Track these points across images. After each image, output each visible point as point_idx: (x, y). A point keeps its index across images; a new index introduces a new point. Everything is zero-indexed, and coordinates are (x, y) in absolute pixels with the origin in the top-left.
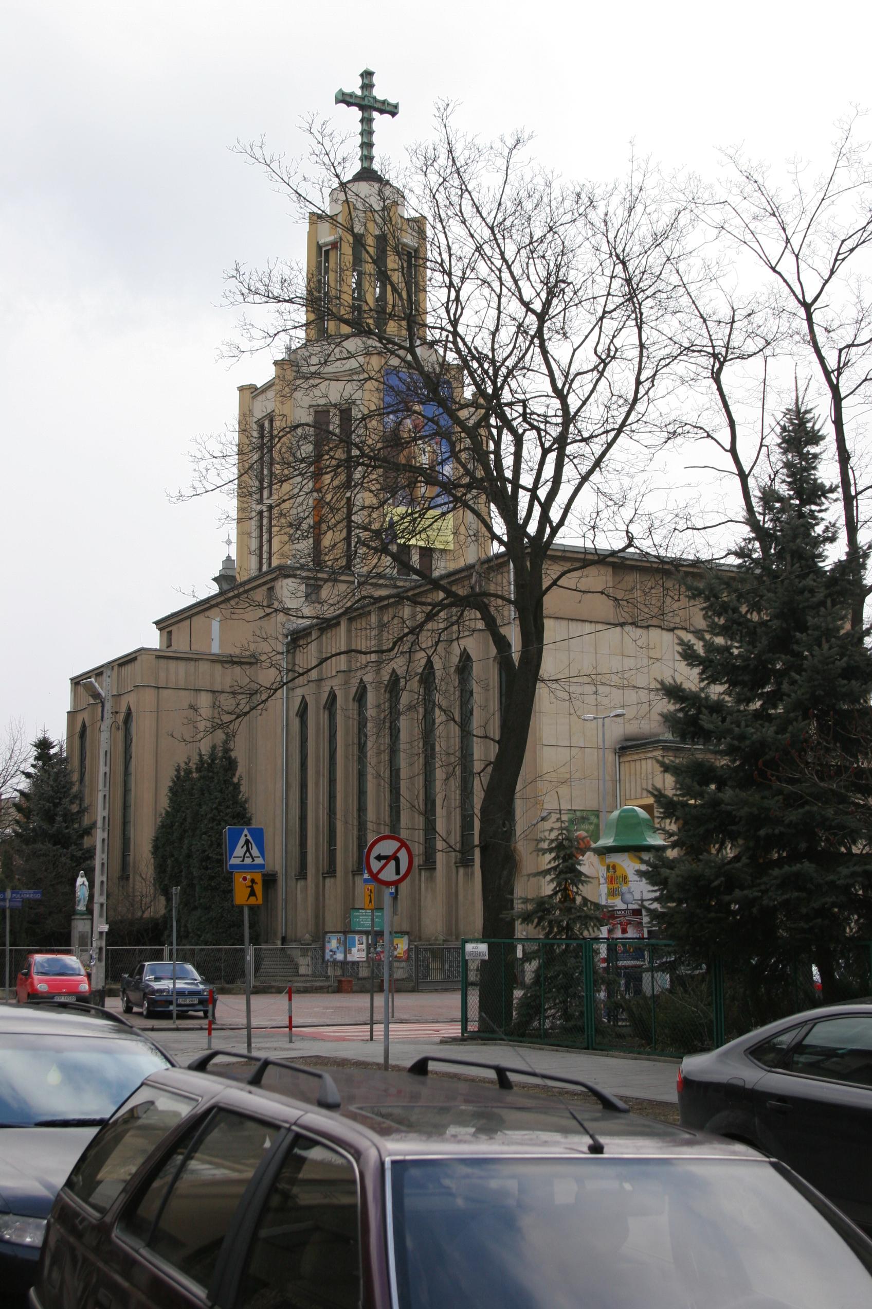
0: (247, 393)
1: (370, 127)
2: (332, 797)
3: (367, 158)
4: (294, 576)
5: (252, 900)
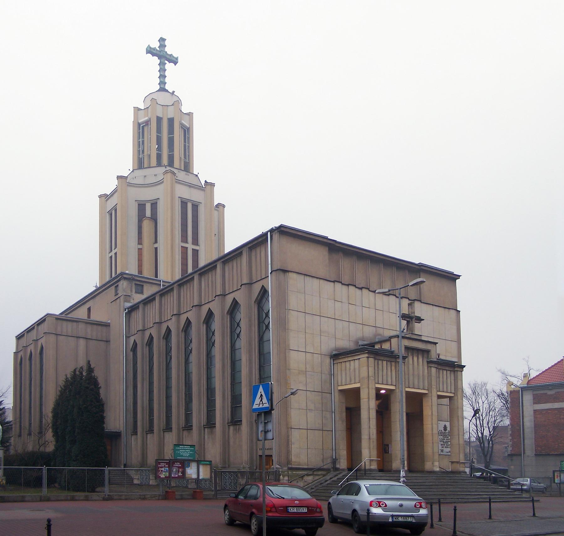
0: (103, 198)
1: (164, 67)
2: (151, 392)
3: (162, 83)
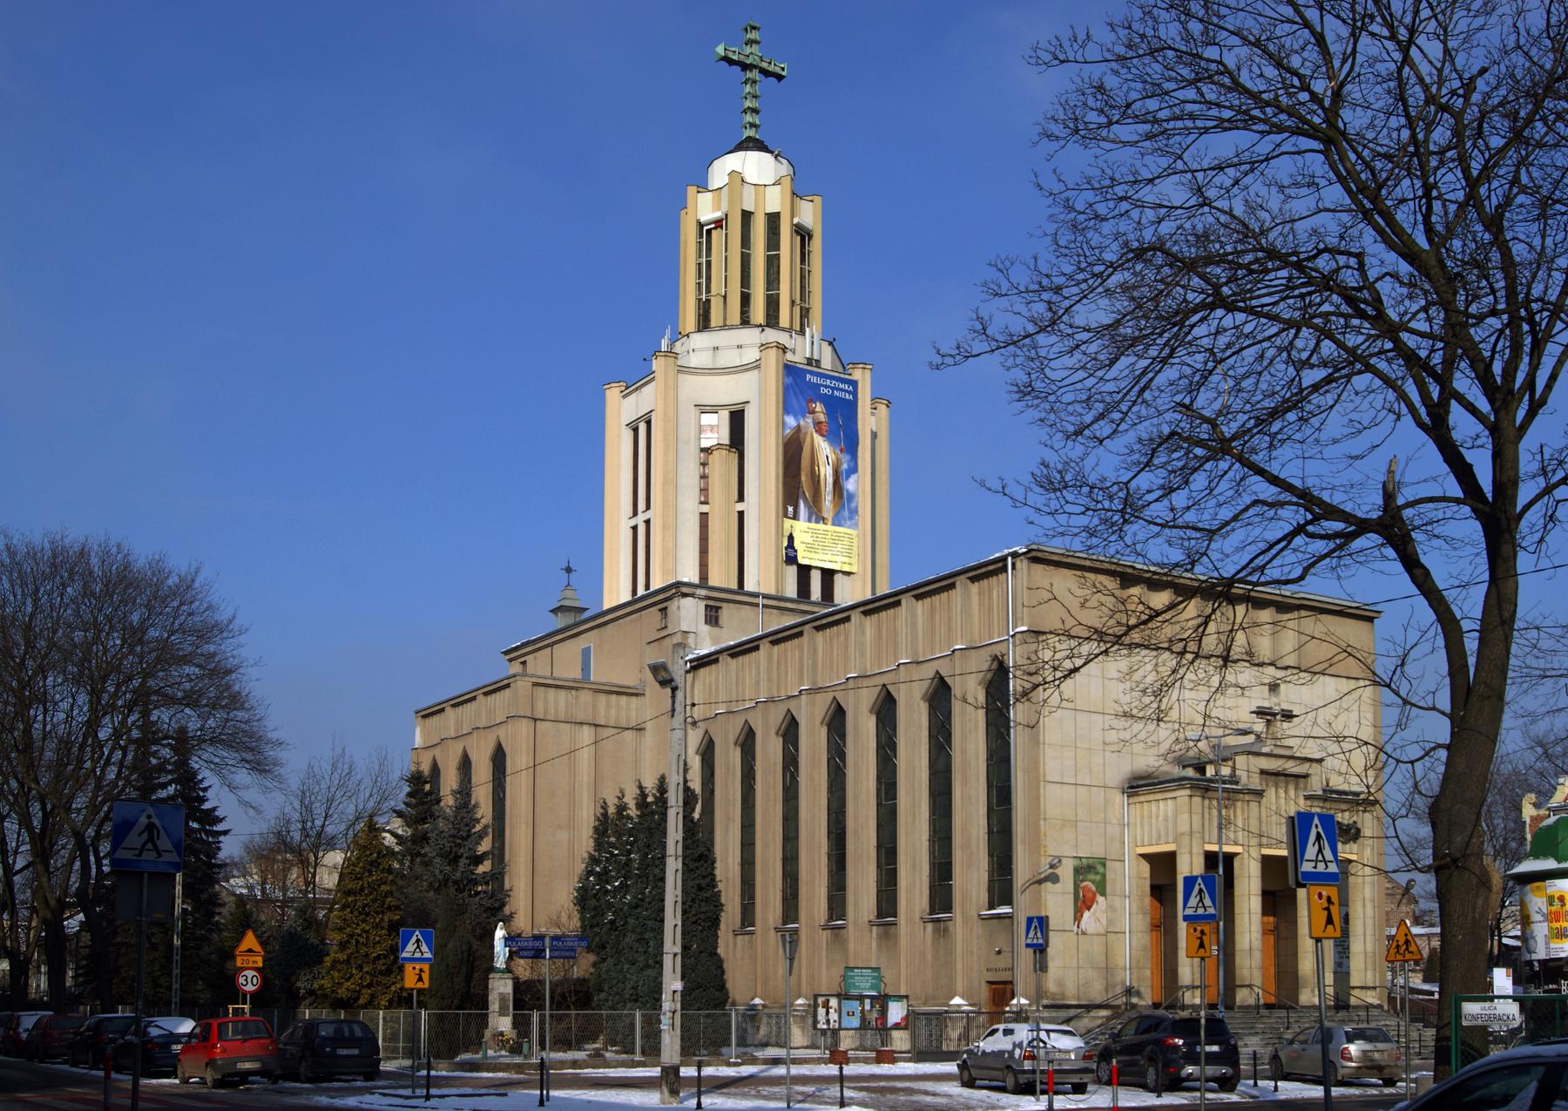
4: (692, 595)
5: (420, 985)
